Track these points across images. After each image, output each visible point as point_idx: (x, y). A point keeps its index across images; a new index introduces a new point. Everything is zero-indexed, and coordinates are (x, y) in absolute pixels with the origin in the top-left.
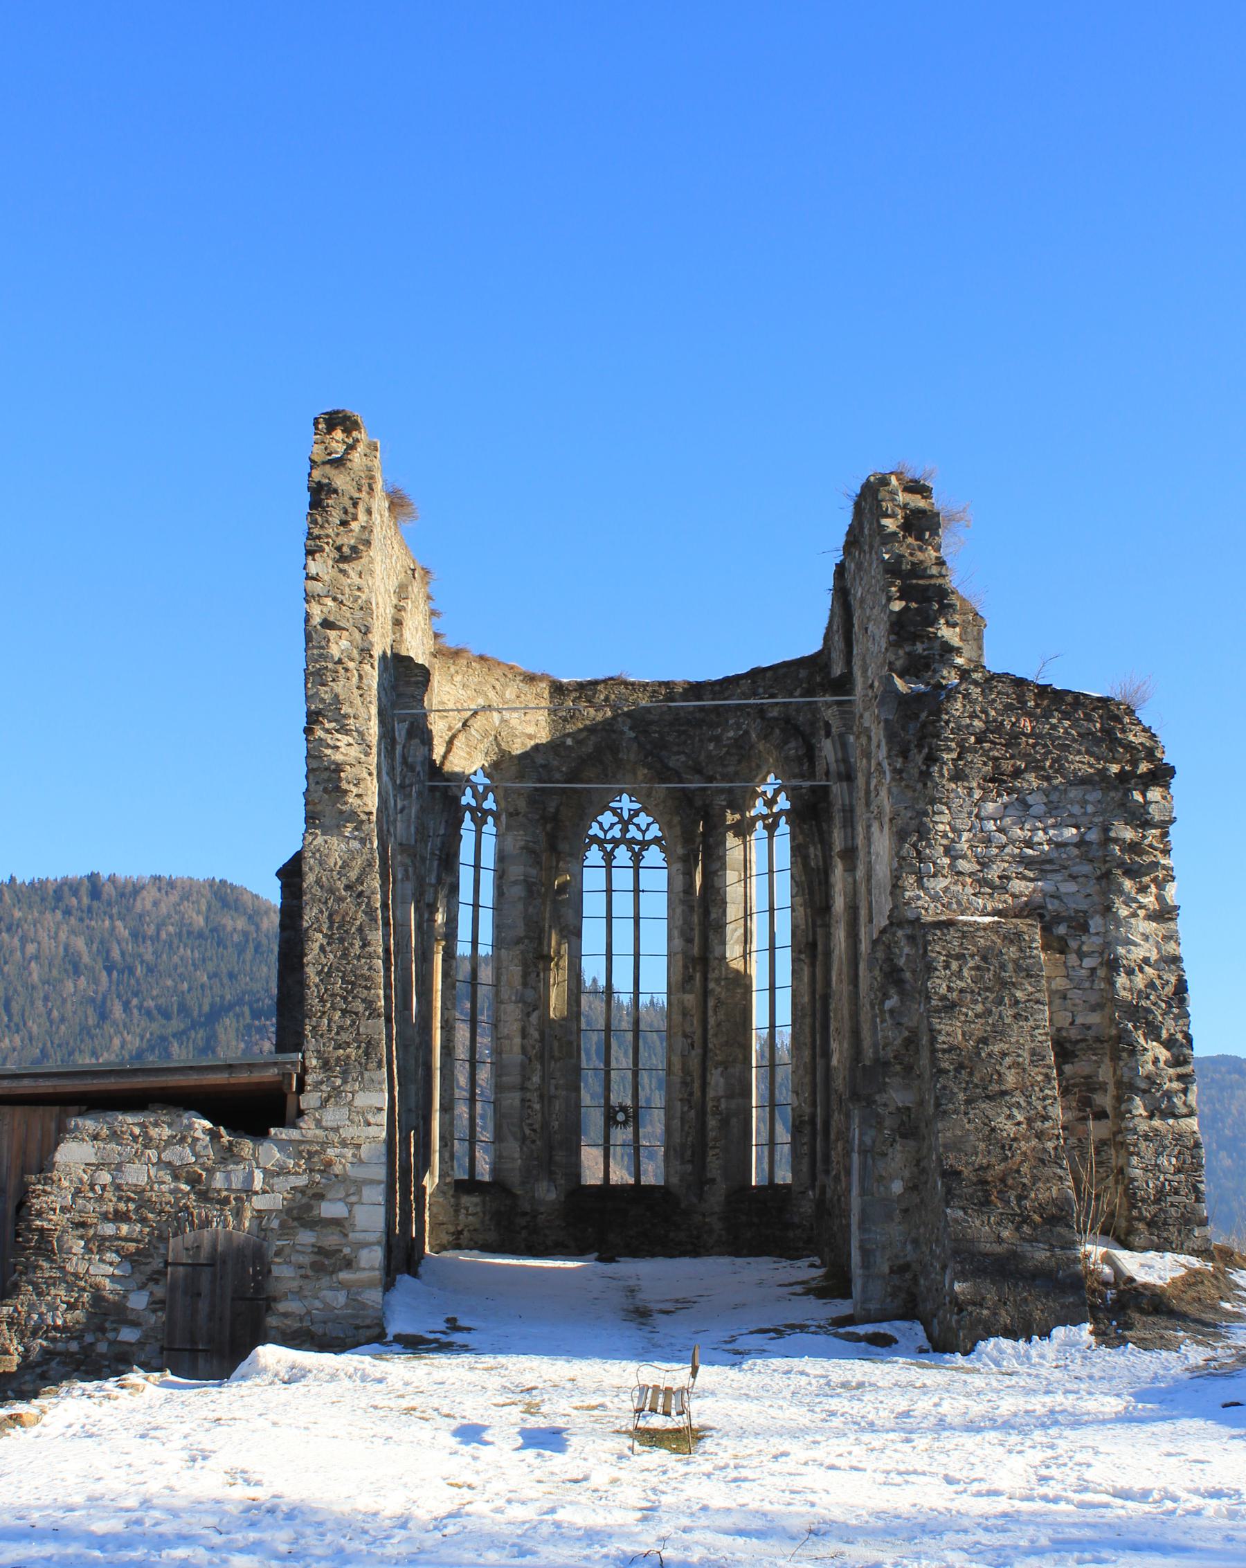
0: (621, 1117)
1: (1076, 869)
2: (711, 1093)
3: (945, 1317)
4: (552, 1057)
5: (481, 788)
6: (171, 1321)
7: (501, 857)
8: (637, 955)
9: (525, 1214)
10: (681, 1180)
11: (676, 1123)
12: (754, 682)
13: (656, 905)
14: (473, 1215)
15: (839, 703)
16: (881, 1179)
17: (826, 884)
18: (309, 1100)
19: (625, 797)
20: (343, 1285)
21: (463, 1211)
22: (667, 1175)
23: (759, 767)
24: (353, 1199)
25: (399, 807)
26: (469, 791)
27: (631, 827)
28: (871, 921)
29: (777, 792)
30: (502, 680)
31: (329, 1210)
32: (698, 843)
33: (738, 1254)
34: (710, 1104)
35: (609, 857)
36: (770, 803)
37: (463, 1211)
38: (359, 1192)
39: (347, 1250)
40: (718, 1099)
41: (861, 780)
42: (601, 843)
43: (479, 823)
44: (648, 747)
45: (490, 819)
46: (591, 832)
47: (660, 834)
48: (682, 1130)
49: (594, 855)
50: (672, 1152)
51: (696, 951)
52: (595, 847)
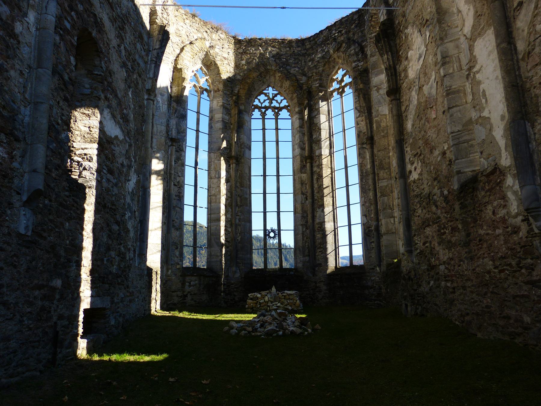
0: (272, 235)
4: (237, 205)
8: (278, 158)
10: (303, 265)
11: (300, 236)
13: (286, 135)
14: (193, 286)
19: (270, 88)
21: (187, 284)
22: (296, 262)
23: (334, 67)
27: (273, 101)
29: (344, 75)
30: (211, 29)
32: (307, 101)
33: (93, 224)
34: (317, 226)
35: (263, 115)
36: (342, 80)
37: (187, 284)
42: (260, 108)
44: (281, 65)
46: (255, 104)
47: (287, 104)
48: (303, 240)
49: (256, 114)
50: (298, 252)
51: (307, 153)
52: (256, 110)
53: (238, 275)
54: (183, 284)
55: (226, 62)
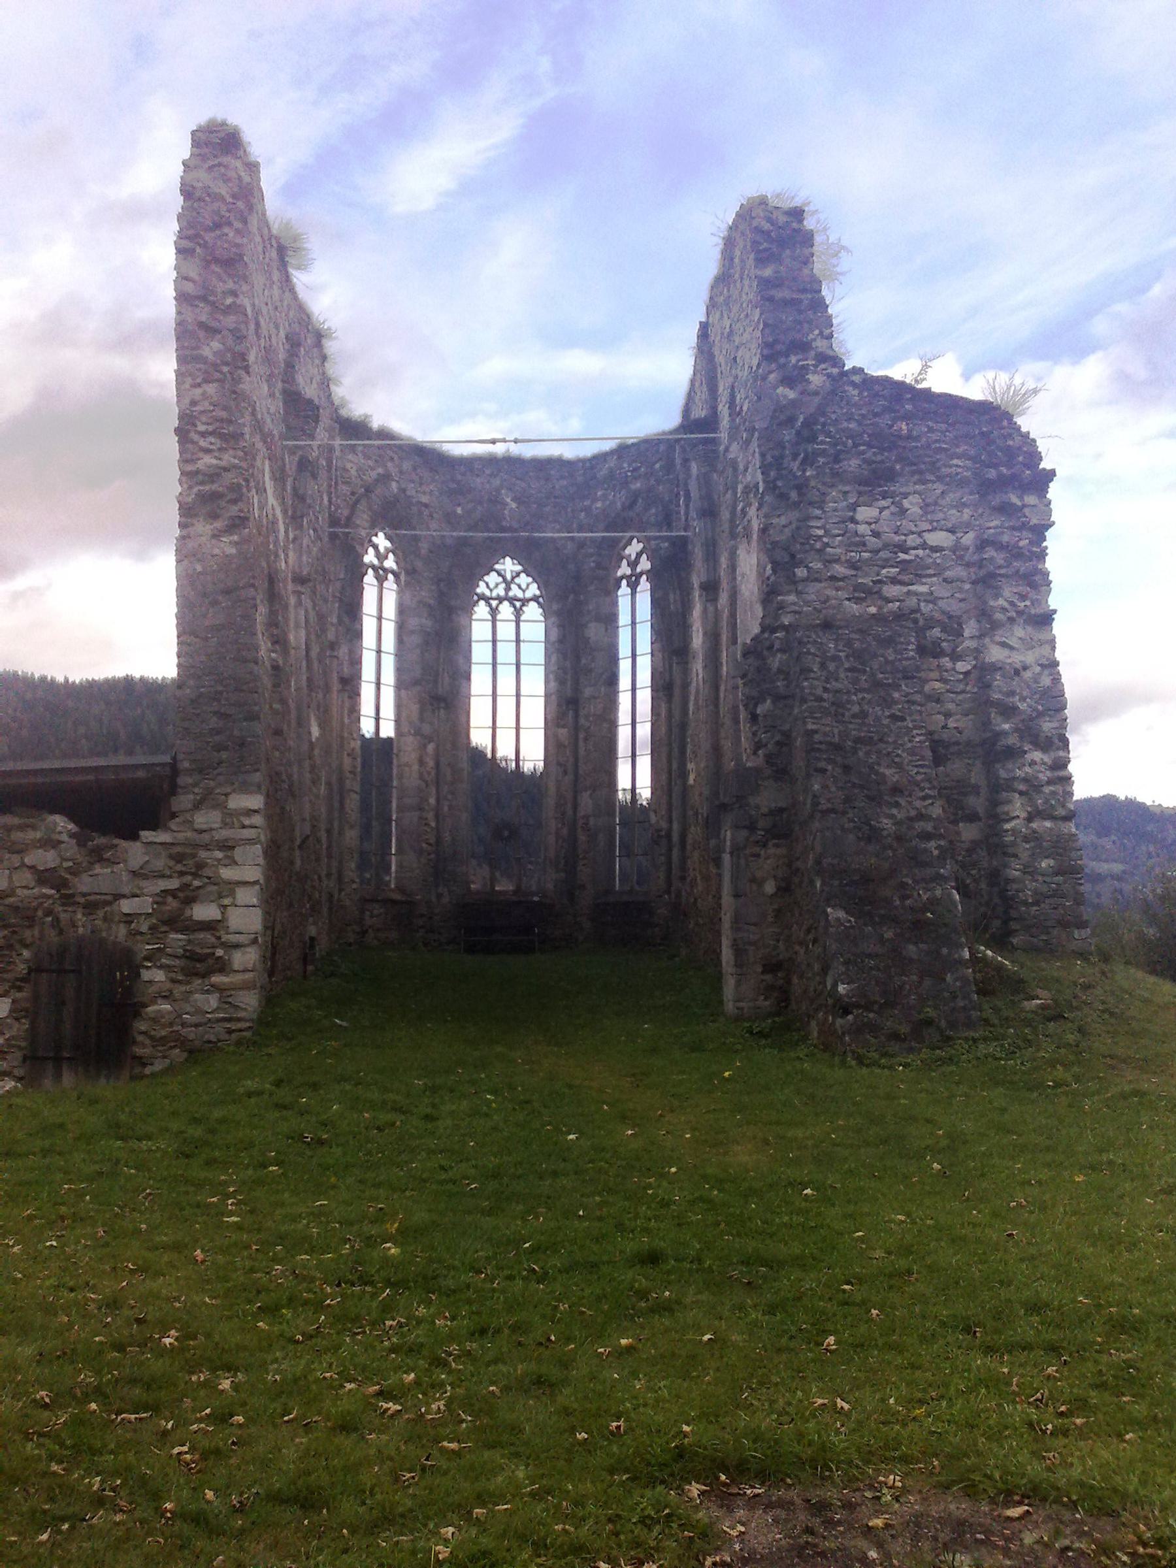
1: (948, 574)
2: (581, 813)
3: (826, 1019)
5: (382, 550)
6: (33, 1028)
7: (402, 610)
8: (518, 695)
9: (422, 916)
12: (619, 458)
13: (535, 653)
15: (706, 441)
16: (753, 880)
17: (685, 627)
18: (182, 801)
20: (216, 988)
24: (226, 901)
25: (291, 536)
26: (371, 550)
27: (513, 586)
28: (735, 642)
29: (639, 555)
31: (204, 912)
34: (581, 822)
35: (494, 612)
36: (633, 564)
37: (368, 913)
38: (232, 893)
39: (220, 952)
40: (587, 817)
41: (725, 515)
42: (487, 600)
43: (381, 580)
45: (390, 576)
46: (479, 590)
49: (481, 610)
52: (482, 603)
53: (446, 900)
54: (362, 912)
55: (426, 512)
